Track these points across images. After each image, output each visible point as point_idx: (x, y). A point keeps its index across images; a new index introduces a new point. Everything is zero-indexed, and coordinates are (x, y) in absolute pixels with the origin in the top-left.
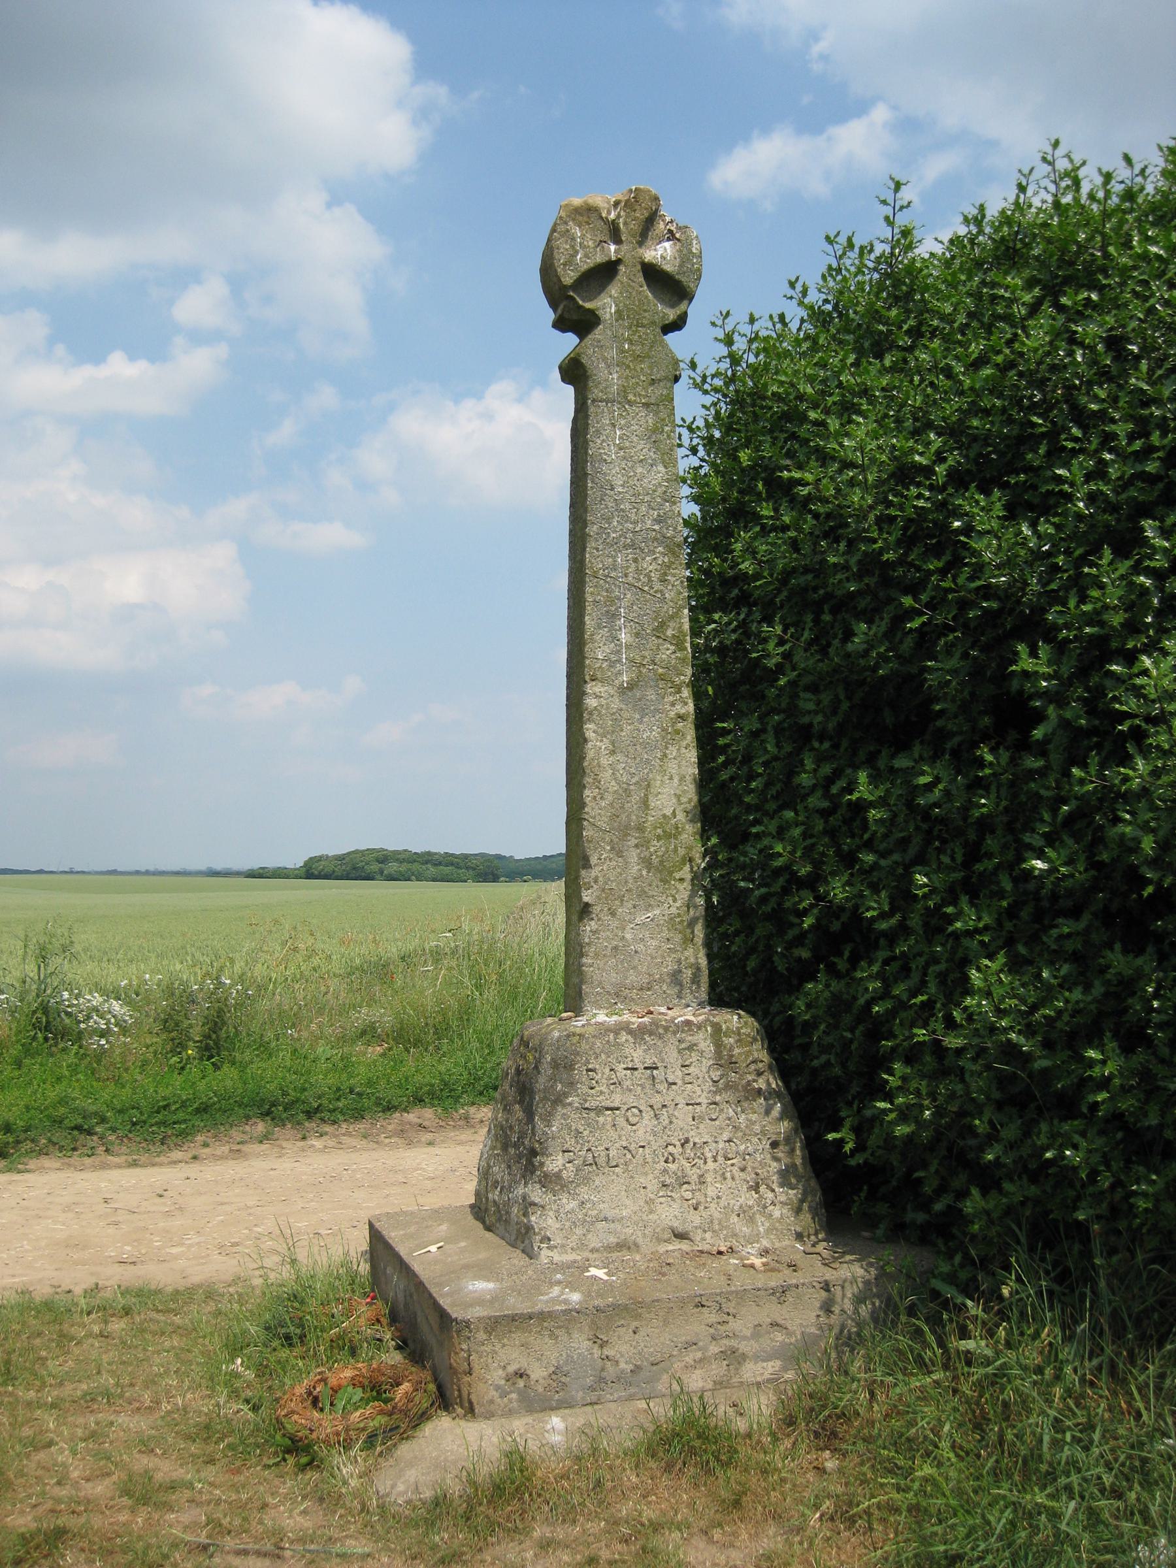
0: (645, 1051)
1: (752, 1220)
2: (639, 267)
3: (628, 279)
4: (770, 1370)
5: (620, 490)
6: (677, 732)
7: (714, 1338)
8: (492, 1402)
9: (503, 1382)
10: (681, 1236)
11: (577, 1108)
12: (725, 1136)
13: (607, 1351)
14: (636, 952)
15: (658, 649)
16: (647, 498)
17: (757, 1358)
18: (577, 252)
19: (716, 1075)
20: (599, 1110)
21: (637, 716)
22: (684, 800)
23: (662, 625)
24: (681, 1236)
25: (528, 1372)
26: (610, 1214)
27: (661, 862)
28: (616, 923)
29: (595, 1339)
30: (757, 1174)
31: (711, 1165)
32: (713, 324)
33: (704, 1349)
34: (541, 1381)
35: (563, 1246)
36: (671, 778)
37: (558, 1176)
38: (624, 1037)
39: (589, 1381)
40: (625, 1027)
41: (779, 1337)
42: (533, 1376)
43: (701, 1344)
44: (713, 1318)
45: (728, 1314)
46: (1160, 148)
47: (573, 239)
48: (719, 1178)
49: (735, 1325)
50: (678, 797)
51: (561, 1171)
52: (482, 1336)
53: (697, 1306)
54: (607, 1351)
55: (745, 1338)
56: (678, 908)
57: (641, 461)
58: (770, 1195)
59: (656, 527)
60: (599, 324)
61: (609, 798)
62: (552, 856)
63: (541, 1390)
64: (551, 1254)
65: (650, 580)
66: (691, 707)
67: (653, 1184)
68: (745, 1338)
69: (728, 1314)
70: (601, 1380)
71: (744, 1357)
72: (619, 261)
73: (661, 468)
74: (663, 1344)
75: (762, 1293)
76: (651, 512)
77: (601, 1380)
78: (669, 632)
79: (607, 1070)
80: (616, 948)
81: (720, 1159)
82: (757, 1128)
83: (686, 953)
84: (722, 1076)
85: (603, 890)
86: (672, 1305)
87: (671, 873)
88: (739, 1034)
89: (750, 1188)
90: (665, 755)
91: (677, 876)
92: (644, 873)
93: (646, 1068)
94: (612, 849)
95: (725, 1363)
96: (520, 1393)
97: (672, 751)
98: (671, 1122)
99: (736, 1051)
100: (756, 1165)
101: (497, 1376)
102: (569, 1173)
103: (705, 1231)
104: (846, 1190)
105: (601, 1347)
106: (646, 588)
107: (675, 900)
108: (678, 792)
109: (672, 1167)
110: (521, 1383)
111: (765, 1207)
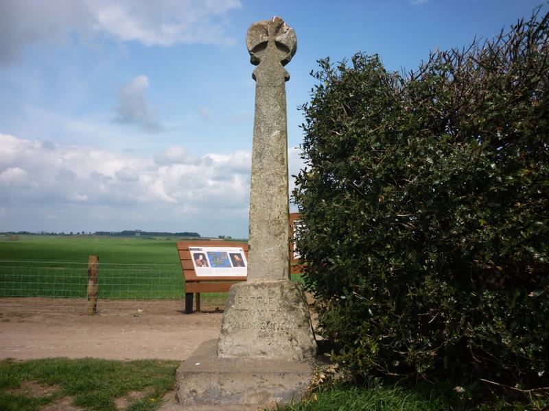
1: (288, 350)
3: (271, 47)
7: (259, 387)
8: (184, 399)
10: (264, 353)
17: (274, 396)
19: (281, 302)
20: (242, 310)
24: (264, 353)
29: (219, 382)
31: (276, 331)
32: (512, 26)
33: (255, 391)
39: (216, 396)
44: (259, 380)
49: (266, 384)
52: (183, 377)
58: (295, 342)
67: (256, 335)
71: (269, 395)
72: (267, 42)
73: (279, 107)
77: (221, 396)
89: (289, 340)
96: (194, 397)
101: (187, 391)
102: (230, 330)
110: (194, 394)
111: (293, 346)
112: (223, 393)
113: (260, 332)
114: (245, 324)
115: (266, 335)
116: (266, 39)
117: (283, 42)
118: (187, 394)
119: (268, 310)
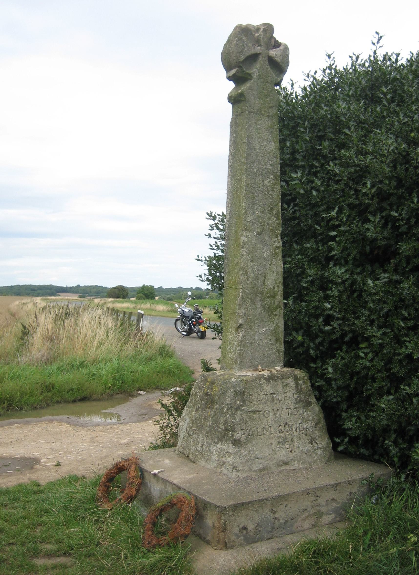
0: (271, 387)
2: (267, 58)
4: (331, 518)
5: (258, 151)
6: (276, 253)
8: (234, 541)
9: (238, 532)
11: (246, 411)
12: (300, 422)
13: (276, 516)
14: (259, 345)
15: (270, 219)
16: (267, 155)
18: (245, 48)
21: (262, 246)
22: (278, 282)
23: (272, 209)
25: (247, 527)
26: (259, 455)
27: (269, 307)
28: (252, 333)
30: (311, 437)
31: (295, 434)
34: (252, 530)
35: (243, 470)
36: (273, 273)
37: (239, 440)
38: (263, 381)
39: (269, 529)
40: (261, 377)
41: (334, 504)
42: (249, 529)
43: (308, 509)
45: (318, 496)
46: (252, 57)
47: (244, 42)
48: (299, 439)
49: (320, 501)
50: (276, 280)
51: (240, 438)
52: (231, 513)
53: (307, 494)
54: (276, 516)
55: (323, 506)
56: (274, 327)
57: (266, 139)
59: (271, 168)
60: (251, 80)
61: (250, 280)
62: (15, 286)
63: (252, 534)
64: (238, 474)
65: (268, 190)
66: (281, 244)
68: (323, 506)
69: (318, 496)
70: (273, 528)
71: (322, 514)
72: (260, 54)
73: (273, 143)
74: (295, 511)
75: (329, 487)
76: (269, 161)
78: (274, 212)
79: (257, 395)
80: (251, 343)
81: (298, 430)
82: (311, 418)
83: (277, 345)
84: (298, 397)
85: (247, 318)
86: (299, 494)
87: (272, 312)
88: (304, 379)
90: (271, 263)
91: (274, 313)
92: (263, 312)
93: (271, 394)
94: (251, 302)
95: (316, 517)
97: (274, 262)
98: (280, 416)
99: (303, 386)
100: (311, 433)
101: (236, 530)
102: (243, 439)
103: (294, 461)
104: (344, 443)
105: (274, 514)
106: (266, 193)
107: (273, 324)
108: (276, 279)
109: (282, 435)
110: (245, 532)
112: (277, 523)
113: (279, 437)
114: (259, 430)
115: (285, 441)
116: (258, 49)
117: (278, 59)
118: (236, 535)
119: (285, 408)
